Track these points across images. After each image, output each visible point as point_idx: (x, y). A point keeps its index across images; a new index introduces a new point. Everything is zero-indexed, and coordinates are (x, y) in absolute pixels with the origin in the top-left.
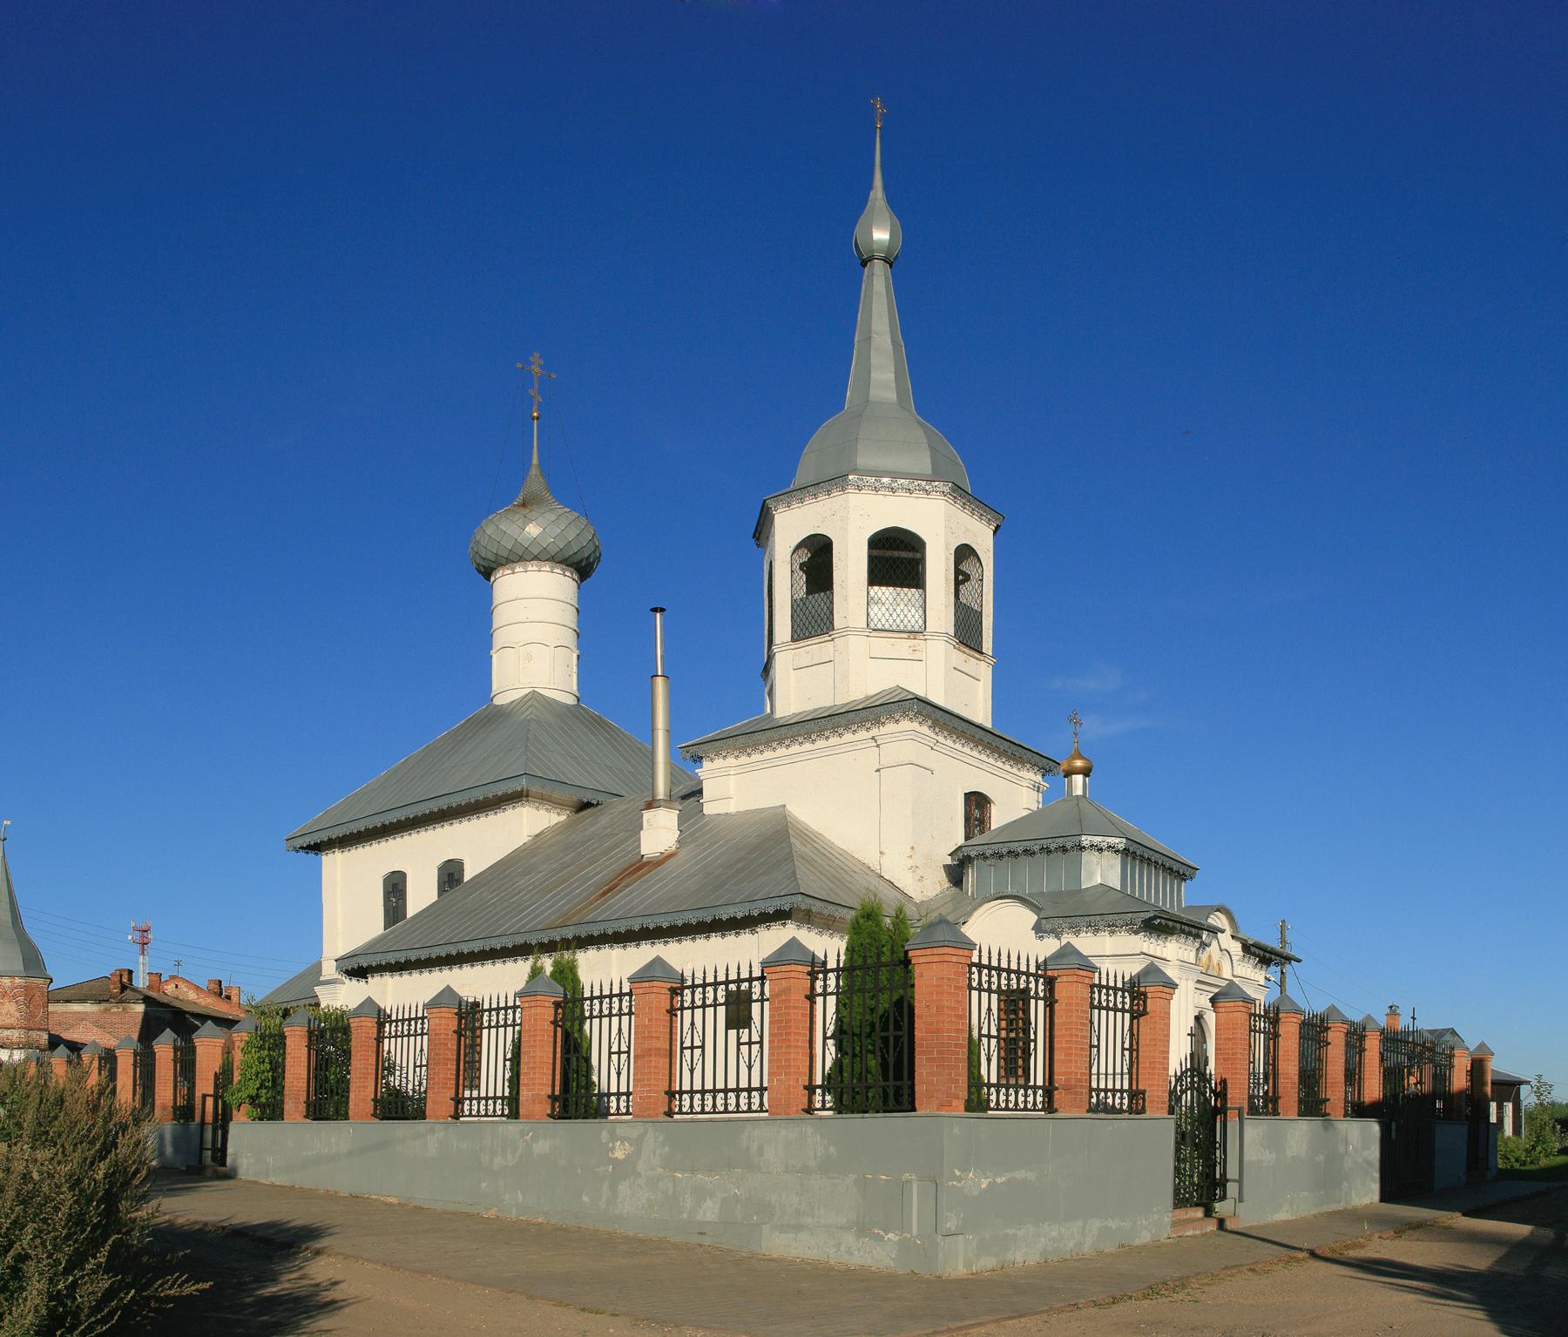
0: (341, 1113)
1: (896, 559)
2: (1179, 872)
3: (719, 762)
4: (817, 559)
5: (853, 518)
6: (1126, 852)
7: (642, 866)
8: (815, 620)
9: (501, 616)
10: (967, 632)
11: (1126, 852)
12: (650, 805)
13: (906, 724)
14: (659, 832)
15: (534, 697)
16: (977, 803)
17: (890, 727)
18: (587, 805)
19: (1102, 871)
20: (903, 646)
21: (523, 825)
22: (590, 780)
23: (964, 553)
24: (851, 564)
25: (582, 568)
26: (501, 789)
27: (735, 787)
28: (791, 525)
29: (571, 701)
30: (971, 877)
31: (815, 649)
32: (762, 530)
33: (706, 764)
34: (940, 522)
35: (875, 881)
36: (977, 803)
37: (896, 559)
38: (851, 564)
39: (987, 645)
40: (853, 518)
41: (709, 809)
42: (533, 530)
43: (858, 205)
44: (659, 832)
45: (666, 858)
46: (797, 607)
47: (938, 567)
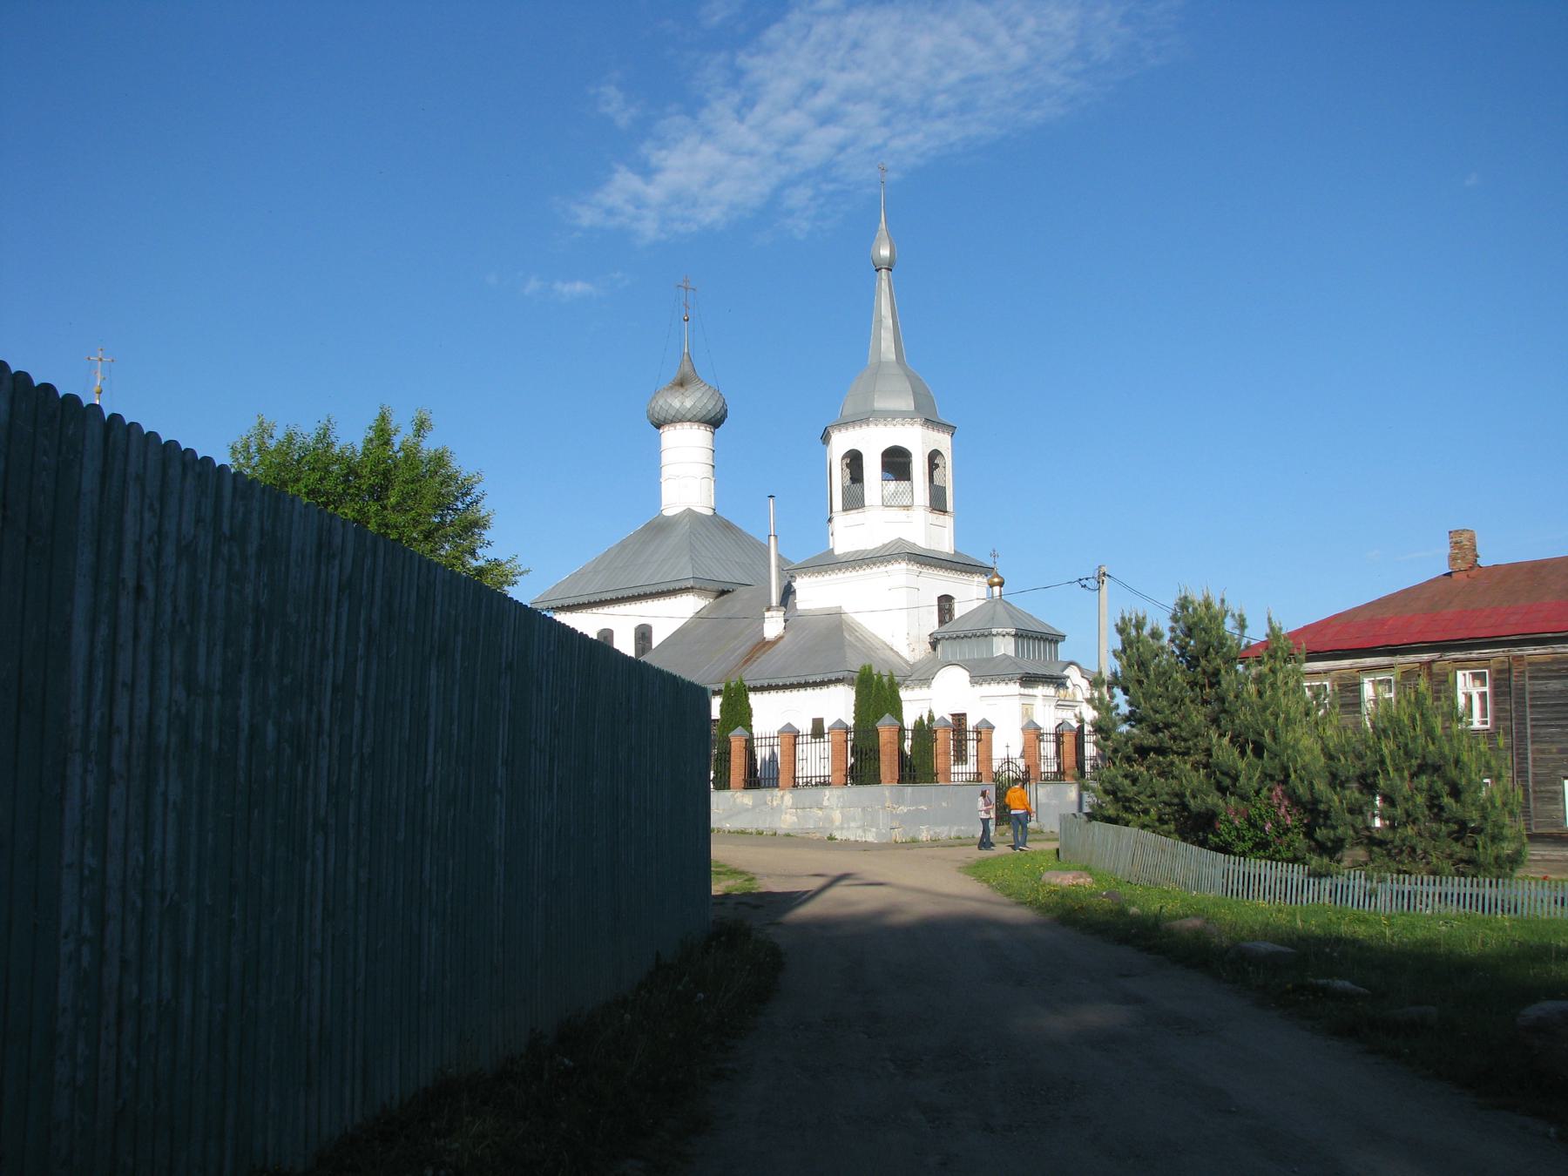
0: (875, 779)
1: (896, 463)
2: (1054, 639)
3: (806, 579)
4: (854, 461)
5: (872, 441)
6: (1016, 635)
7: (764, 645)
8: (854, 501)
9: (666, 457)
10: (937, 502)
11: (1016, 635)
12: (768, 610)
13: (903, 565)
14: (773, 626)
15: (690, 513)
16: (945, 603)
17: (896, 566)
18: (723, 593)
19: (1004, 647)
20: (902, 514)
21: (686, 607)
22: (725, 576)
23: (934, 458)
24: (872, 467)
25: (714, 422)
26: (677, 586)
27: (813, 594)
28: (842, 442)
29: (710, 513)
30: (939, 648)
31: (854, 515)
32: (826, 438)
33: (799, 580)
34: (917, 440)
35: (888, 652)
36: (945, 603)
37: (896, 463)
38: (872, 467)
39: (950, 506)
40: (872, 441)
41: (800, 606)
42: (688, 404)
43: (870, 237)
44: (773, 626)
45: (780, 638)
46: (846, 492)
47: (919, 467)
